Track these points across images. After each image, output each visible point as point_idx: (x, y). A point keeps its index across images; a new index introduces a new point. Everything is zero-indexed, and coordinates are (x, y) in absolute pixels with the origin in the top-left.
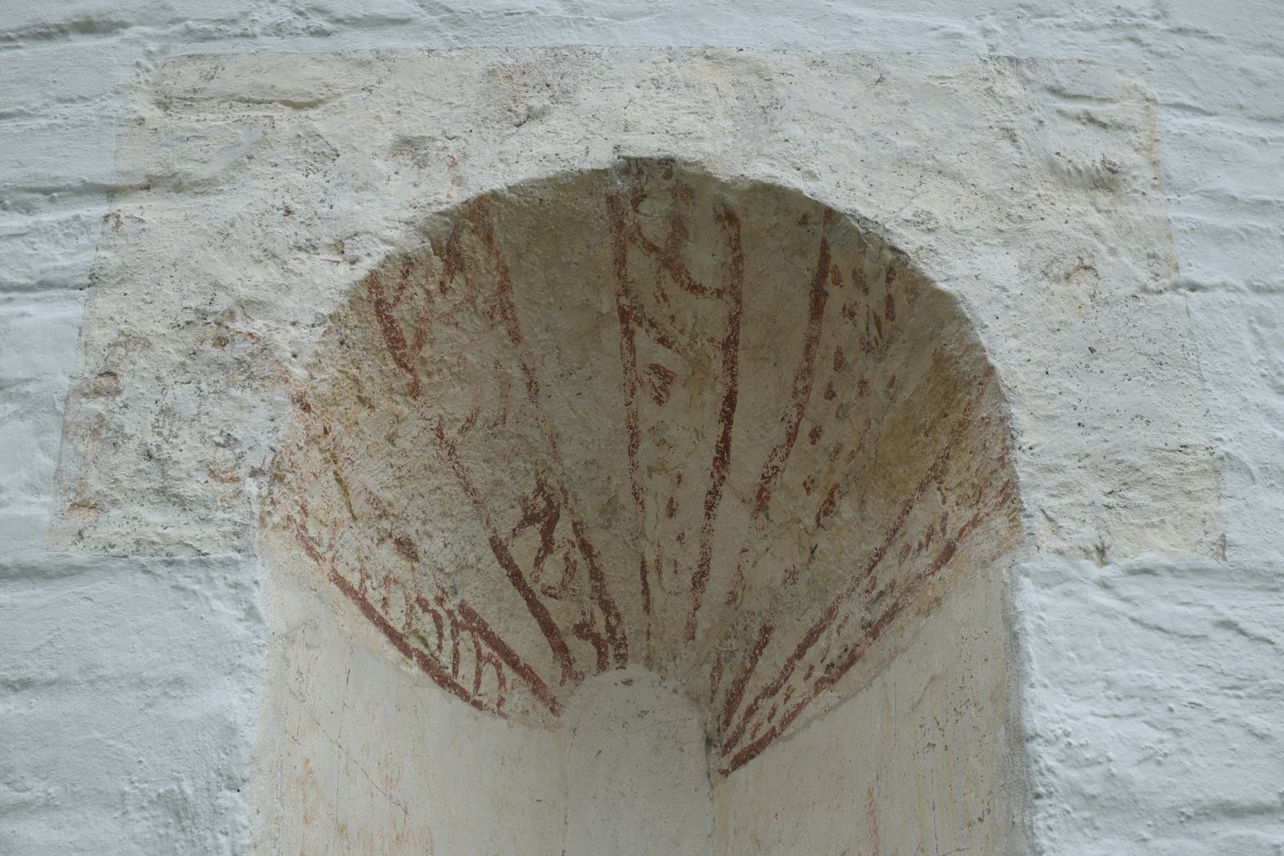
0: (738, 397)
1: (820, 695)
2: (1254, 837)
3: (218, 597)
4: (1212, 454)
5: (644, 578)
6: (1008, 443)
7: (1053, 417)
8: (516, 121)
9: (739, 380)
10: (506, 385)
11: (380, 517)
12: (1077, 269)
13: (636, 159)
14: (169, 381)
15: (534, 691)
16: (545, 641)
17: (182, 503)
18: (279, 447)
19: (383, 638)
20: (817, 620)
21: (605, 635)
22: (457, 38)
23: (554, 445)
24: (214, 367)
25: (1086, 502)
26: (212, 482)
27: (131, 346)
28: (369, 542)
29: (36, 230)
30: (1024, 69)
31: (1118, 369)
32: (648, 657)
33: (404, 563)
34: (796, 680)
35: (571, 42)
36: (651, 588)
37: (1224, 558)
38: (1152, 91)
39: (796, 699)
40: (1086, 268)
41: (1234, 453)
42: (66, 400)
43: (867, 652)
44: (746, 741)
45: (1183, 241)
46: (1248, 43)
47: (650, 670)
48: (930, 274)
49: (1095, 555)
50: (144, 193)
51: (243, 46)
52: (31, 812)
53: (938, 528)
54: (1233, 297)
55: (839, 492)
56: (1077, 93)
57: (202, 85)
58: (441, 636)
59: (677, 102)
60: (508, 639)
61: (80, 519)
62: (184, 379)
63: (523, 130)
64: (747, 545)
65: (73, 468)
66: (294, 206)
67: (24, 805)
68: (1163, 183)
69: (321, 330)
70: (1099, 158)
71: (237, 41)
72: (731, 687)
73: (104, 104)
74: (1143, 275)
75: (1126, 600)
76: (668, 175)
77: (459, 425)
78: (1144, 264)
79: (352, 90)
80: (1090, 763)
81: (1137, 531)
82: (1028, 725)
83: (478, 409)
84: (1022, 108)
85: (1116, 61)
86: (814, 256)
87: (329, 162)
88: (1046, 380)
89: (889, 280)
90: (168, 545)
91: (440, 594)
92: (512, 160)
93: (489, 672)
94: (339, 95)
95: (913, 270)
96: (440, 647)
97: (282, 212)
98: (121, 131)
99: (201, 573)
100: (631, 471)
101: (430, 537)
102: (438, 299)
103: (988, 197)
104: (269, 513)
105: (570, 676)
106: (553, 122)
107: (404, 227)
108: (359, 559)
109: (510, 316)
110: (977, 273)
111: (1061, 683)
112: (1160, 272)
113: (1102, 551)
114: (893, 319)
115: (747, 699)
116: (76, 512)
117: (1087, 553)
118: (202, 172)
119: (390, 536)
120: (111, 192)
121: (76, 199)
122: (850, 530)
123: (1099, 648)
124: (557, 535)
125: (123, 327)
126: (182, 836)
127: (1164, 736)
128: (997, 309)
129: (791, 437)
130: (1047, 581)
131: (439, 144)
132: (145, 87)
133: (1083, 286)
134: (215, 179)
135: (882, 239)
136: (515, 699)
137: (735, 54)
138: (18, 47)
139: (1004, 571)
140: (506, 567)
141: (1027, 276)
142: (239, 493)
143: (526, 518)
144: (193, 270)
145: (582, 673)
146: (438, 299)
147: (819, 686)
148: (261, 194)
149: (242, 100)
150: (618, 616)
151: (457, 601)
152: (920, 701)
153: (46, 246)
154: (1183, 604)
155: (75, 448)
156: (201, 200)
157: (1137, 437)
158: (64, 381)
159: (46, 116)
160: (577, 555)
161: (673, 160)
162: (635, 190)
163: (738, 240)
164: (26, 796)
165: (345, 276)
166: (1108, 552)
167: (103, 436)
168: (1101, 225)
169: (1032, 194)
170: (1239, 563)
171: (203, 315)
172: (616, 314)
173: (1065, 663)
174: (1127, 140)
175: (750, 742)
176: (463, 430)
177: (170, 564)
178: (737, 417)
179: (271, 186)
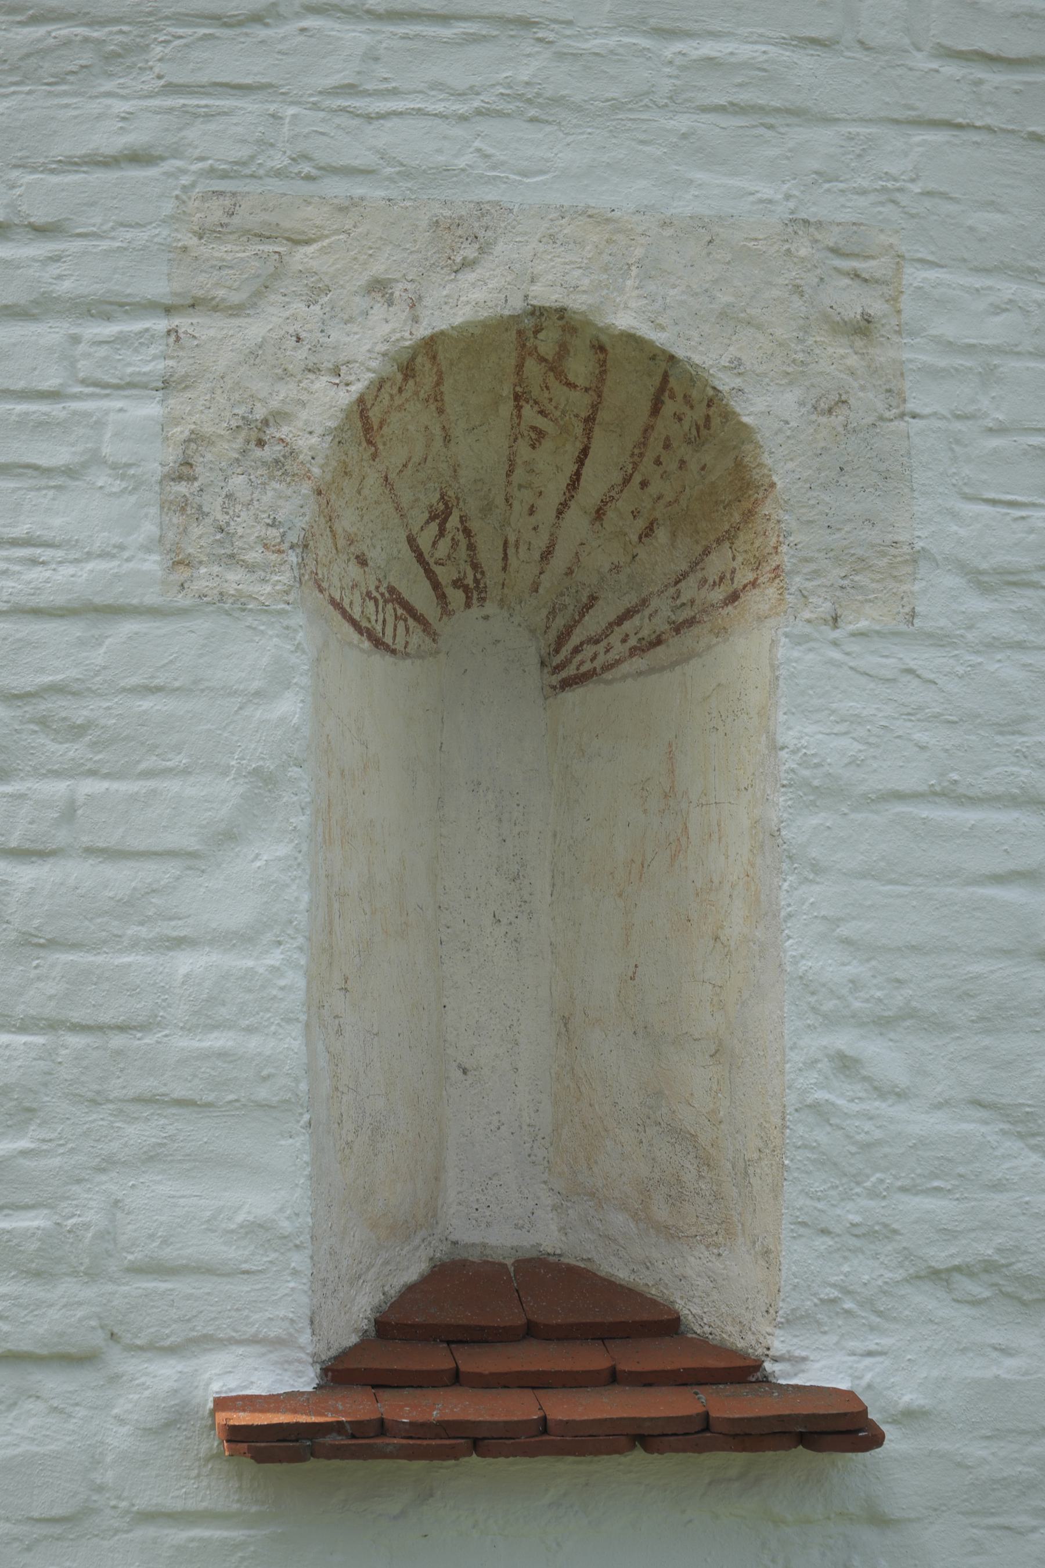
0: (591, 450)
1: (634, 659)
4: (912, 548)
6: (781, 539)
7: (812, 522)
8: (455, 268)
9: (593, 440)
12: (836, 404)
13: (540, 307)
16: (432, 593)
20: (633, 603)
21: (472, 585)
23: (455, 471)
30: (812, 230)
32: (501, 600)
34: (615, 639)
36: (509, 557)
37: (913, 625)
39: (613, 655)
41: (928, 547)
43: (670, 641)
44: (571, 671)
47: (502, 608)
50: (191, 310)
52: (174, 775)
53: (728, 576)
55: (658, 524)
56: (849, 252)
58: (377, 612)
61: (182, 574)
62: (239, 471)
63: (460, 276)
64: (585, 541)
70: (859, 311)
71: (248, 181)
72: (561, 628)
75: (848, 654)
76: (561, 318)
83: (410, 458)
86: (657, 380)
88: (810, 494)
89: (709, 406)
90: (242, 597)
97: (294, 339)
98: (171, 256)
103: (780, 345)
109: (439, 399)
112: (892, 404)
113: (835, 619)
114: (709, 429)
115: (575, 640)
120: (169, 310)
122: (663, 551)
124: (448, 525)
129: (627, 481)
135: (707, 380)
137: (610, 215)
140: (414, 551)
141: (803, 410)
145: (453, 610)
147: (633, 651)
149: (255, 235)
150: (483, 573)
152: (709, 696)
155: (170, 520)
160: (461, 536)
162: (536, 326)
163: (605, 361)
165: (345, 397)
166: (839, 620)
167: (189, 512)
172: (512, 396)
175: (575, 672)
178: (587, 462)
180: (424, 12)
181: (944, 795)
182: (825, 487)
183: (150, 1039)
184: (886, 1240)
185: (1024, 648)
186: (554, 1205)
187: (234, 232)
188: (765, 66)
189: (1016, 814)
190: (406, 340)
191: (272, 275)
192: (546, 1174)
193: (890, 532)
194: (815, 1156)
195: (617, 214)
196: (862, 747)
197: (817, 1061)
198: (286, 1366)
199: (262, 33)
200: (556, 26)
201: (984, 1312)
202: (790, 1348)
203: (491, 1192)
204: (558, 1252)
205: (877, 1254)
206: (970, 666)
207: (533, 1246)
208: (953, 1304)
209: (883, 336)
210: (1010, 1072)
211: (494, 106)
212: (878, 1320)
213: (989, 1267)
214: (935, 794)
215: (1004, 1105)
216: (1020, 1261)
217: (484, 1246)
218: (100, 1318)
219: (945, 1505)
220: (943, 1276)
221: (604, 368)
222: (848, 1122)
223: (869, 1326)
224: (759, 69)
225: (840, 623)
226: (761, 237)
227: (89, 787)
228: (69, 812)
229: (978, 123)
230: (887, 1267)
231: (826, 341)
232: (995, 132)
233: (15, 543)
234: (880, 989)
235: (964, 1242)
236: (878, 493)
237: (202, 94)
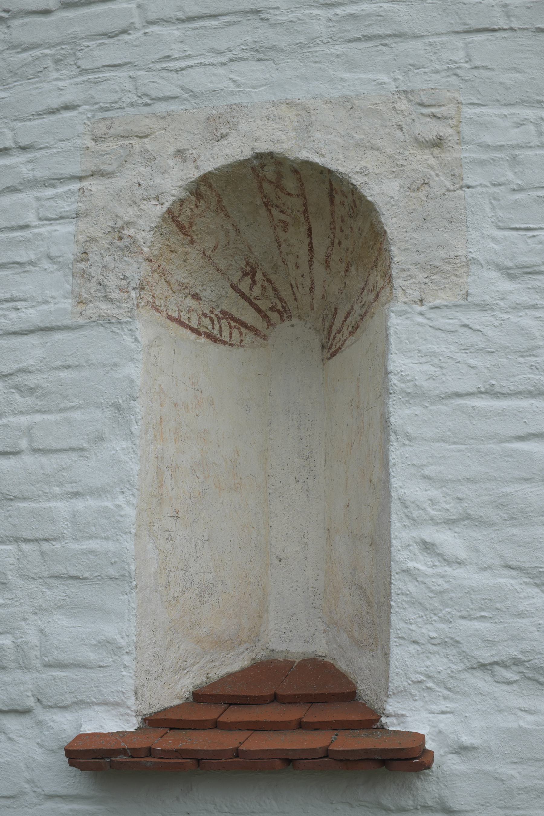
0: (312, 229)
2: (466, 404)
3: (125, 335)
5: (292, 289)
7: (407, 249)
8: (217, 139)
10: (227, 232)
11: (184, 289)
12: (422, 185)
13: (260, 153)
14: (104, 255)
15: (255, 334)
16: (258, 315)
17: (111, 300)
18: (141, 278)
19: (189, 332)
21: (282, 310)
22: (196, 103)
23: (250, 249)
24: (119, 249)
25: (417, 282)
26: (121, 293)
27: (91, 242)
28: (181, 299)
29: (57, 196)
31: (435, 226)
32: (299, 316)
33: (195, 302)
35: (236, 102)
37: (467, 300)
38: (461, 99)
40: (426, 184)
42: (72, 264)
44: (333, 349)
45: (466, 167)
46: (505, 68)
47: (301, 320)
48: (365, 194)
49: (419, 303)
50: (91, 178)
51: (120, 113)
54: (484, 190)
57: (107, 131)
58: (213, 324)
59: (275, 126)
60: (242, 318)
61: (81, 308)
62: (109, 254)
63: (220, 143)
65: (77, 289)
66: (142, 182)
67: (73, 407)
68: (461, 142)
69: (152, 232)
70: (435, 134)
71: (119, 110)
73: (75, 141)
74: (448, 184)
75: (428, 319)
77: (211, 249)
78: (449, 179)
79: (160, 129)
80: (409, 381)
81: (435, 292)
82: (389, 368)
83: (218, 243)
84: (406, 114)
85: (448, 86)
87: (152, 162)
88: (406, 234)
89: (353, 194)
91: (212, 309)
92: (215, 156)
93: (235, 332)
94: (155, 132)
95: (359, 192)
96: (213, 328)
97: (137, 185)
99: (119, 326)
100: (280, 254)
101: (206, 290)
102: (196, 210)
103: (390, 157)
104: (140, 302)
105: (271, 325)
106: (230, 139)
107: (178, 189)
108: (177, 307)
110: (382, 192)
111: (402, 352)
112: (455, 182)
113: (421, 301)
116: (79, 305)
117: (415, 302)
118: (109, 169)
119: (189, 294)
120: (81, 178)
121: (69, 181)
123: (417, 338)
125: (88, 234)
126: (120, 416)
127: (436, 369)
128: (389, 206)
129: (333, 243)
130: (400, 314)
131: (190, 152)
132: (88, 133)
133: (424, 192)
134: (114, 171)
136: (248, 339)
137: (297, 102)
138: (44, 118)
139: (386, 310)
140: (238, 293)
141: (402, 190)
142: (129, 297)
143: (243, 275)
144: (109, 211)
146: (196, 210)
148: (130, 177)
149: (121, 137)
150: (285, 302)
151: (219, 310)
153: (60, 202)
154: (450, 319)
156: (110, 180)
157: (438, 254)
158: (71, 256)
159: (56, 148)
160: (266, 284)
161: (273, 153)
162: (261, 164)
163: (300, 178)
164: (73, 404)
165: (160, 210)
168: (434, 163)
169: (407, 153)
170: (472, 301)
171: (113, 228)
172: (263, 204)
173: (404, 345)
174: (448, 124)
176: (213, 251)
177: (110, 323)
178: (313, 236)
179: (133, 173)
180: (204, 15)
181: (487, 393)
182: (414, 230)
183: (58, 545)
184: (452, 647)
185: (536, 308)
186: (324, 630)
187: (111, 137)
188: (381, 14)
189: (533, 401)
190: (191, 178)
191: (128, 155)
192: (321, 613)
193: (453, 251)
194: (409, 599)
195: (301, 100)
196: (436, 369)
197: (409, 545)
198: (121, 717)
199: (126, 37)
200: (271, 11)
201: (515, 689)
202: (395, 709)
203: (292, 624)
204: (324, 655)
205: (447, 655)
206: (502, 320)
207: (313, 652)
208: (495, 684)
209: (450, 146)
210: (529, 548)
211: (239, 56)
212: (449, 693)
213: (517, 662)
214: (481, 393)
215: (525, 567)
216: (535, 659)
217: (288, 652)
218: (32, 691)
219: (488, 803)
220: (488, 667)
221: (301, 183)
222: (428, 580)
223: (443, 696)
224: (378, 16)
225: (424, 303)
226: (379, 102)
227: (38, 418)
228: (29, 430)
229: (505, 27)
230: (453, 663)
231: (416, 152)
232: (516, 30)
233: (7, 301)
234: (447, 503)
235: (500, 647)
236: (446, 231)
237: (98, 72)
